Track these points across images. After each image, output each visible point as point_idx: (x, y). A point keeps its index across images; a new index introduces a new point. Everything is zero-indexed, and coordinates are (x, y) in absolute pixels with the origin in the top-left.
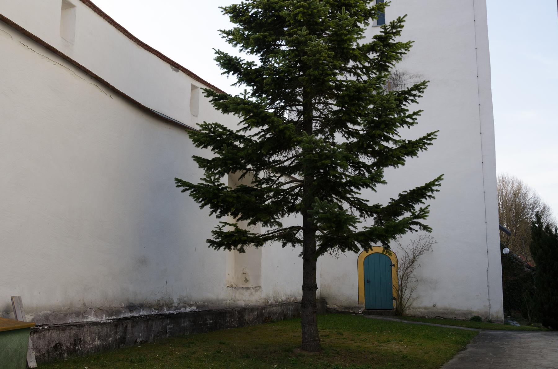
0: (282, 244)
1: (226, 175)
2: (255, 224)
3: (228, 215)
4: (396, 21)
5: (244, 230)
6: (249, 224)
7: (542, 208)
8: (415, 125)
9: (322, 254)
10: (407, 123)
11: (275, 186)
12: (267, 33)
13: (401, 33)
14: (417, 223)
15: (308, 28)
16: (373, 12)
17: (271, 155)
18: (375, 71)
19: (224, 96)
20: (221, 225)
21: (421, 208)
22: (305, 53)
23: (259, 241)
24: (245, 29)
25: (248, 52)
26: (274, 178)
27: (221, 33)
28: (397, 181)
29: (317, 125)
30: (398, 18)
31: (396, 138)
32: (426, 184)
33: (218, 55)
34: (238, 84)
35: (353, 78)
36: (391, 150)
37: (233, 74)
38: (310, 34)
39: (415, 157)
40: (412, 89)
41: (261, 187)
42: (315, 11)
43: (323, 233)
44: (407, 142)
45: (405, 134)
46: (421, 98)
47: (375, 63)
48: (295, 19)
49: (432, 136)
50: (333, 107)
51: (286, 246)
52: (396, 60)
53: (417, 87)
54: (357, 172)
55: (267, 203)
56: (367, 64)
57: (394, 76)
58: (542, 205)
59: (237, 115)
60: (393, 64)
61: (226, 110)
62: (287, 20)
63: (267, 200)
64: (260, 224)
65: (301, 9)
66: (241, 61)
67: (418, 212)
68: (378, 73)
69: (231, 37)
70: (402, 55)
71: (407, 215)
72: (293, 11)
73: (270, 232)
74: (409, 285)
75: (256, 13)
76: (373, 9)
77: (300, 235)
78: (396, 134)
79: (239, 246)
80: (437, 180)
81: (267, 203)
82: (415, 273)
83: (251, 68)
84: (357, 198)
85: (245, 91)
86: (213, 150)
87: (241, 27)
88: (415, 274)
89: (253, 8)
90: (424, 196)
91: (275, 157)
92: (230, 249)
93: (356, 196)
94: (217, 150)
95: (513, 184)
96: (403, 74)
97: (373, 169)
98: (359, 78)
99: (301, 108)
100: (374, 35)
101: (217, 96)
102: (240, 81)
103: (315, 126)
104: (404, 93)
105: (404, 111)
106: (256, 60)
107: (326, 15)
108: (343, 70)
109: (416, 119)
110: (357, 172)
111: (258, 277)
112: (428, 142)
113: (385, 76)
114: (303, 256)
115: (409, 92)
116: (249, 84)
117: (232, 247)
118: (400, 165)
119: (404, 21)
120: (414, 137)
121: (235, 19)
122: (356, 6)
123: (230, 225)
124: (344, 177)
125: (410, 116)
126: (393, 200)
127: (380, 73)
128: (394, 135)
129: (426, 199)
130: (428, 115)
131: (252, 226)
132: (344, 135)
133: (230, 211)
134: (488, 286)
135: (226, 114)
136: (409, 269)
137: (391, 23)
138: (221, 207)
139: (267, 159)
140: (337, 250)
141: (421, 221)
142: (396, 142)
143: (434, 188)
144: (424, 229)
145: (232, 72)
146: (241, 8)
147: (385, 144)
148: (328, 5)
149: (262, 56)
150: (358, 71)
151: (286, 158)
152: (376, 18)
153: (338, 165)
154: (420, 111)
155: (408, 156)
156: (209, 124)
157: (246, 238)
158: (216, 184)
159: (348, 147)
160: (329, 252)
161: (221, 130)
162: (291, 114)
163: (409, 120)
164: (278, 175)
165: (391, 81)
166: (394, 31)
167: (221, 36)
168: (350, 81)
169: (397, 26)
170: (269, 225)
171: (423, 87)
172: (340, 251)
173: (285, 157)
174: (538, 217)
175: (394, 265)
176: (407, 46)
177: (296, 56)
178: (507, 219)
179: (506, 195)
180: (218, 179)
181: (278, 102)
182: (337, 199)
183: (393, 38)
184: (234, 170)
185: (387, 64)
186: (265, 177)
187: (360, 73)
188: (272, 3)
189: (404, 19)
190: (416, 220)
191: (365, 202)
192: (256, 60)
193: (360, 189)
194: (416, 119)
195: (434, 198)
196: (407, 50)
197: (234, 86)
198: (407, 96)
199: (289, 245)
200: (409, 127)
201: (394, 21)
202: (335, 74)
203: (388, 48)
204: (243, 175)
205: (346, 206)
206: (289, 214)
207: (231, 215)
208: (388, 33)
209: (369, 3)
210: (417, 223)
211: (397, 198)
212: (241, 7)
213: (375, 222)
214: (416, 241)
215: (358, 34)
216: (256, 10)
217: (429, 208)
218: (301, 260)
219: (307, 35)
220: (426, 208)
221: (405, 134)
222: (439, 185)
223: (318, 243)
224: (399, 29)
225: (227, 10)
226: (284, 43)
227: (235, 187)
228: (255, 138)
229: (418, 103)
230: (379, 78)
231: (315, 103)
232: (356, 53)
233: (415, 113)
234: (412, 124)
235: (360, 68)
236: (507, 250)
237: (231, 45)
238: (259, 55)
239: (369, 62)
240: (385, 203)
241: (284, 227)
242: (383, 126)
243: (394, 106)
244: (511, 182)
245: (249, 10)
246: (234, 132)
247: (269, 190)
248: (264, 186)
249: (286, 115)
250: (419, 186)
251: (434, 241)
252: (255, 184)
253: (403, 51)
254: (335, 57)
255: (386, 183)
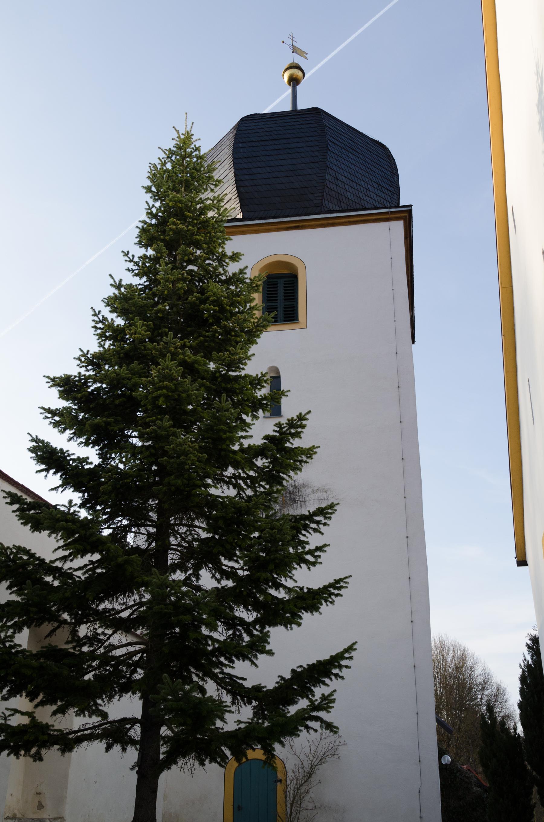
0: (105, 746)
1: (26, 631)
2: (63, 713)
3: (21, 696)
4: (295, 418)
5: (44, 723)
6: (54, 713)
7: (495, 690)
8: (317, 565)
9: (169, 768)
10: (307, 562)
11: (102, 650)
12: (111, 419)
13: (302, 435)
14: (317, 719)
15: (172, 418)
16: (265, 402)
17: (101, 600)
18: (263, 483)
19: (39, 503)
20: (8, 713)
21: (323, 695)
22: (165, 453)
23: (68, 742)
24: (80, 410)
25: (81, 443)
26: (101, 637)
27: (49, 380)
28: (290, 649)
29: (175, 557)
30: (298, 414)
31: (290, 584)
32: (331, 656)
33: (35, 444)
34: (60, 489)
35: (232, 492)
36: (282, 600)
37: (54, 473)
38: (174, 426)
39: (316, 614)
40: (315, 514)
41: (80, 650)
42: (184, 395)
43: (172, 731)
44: (306, 590)
45: (304, 578)
46: (326, 527)
47: (263, 472)
48: (154, 404)
49: (342, 584)
50: (200, 531)
51: (111, 751)
52: (293, 471)
53: (321, 511)
54: (231, 632)
55: (86, 677)
56: (252, 473)
57: (291, 489)
58: (494, 685)
59: (54, 535)
60: (289, 476)
61: (37, 526)
62: (142, 403)
63: (88, 673)
64: (72, 711)
65: (164, 391)
66: (69, 455)
67: (319, 701)
68: (267, 487)
69: (57, 418)
70: (303, 464)
71: (303, 703)
72: (153, 392)
73: (88, 726)
74: (303, 814)
75: (97, 389)
76: (265, 398)
77: (136, 732)
78: (291, 578)
79: (34, 750)
80: (346, 651)
81: (86, 677)
82: (313, 794)
83: (83, 467)
84: (228, 674)
85: (70, 501)
86: (9, 588)
87: (74, 407)
88: (313, 795)
89: (95, 382)
90: (328, 674)
91: (106, 605)
92: (17, 755)
93: (227, 670)
94: (15, 589)
95: (454, 651)
96: (304, 486)
97: (255, 629)
98: (241, 492)
99: (153, 530)
100: (264, 435)
101: (26, 503)
102: (64, 485)
103: (172, 557)
104: (304, 517)
105: (303, 543)
106: (92, 455)
107: (199, 401)
108: (219, 480)
109: (319, 556)
110: (231, 632)
111: (60, 800)
112: (336, 592)
113: (278, 491)
114: (137, 769)
115: (310, 517)
116: (77, 489)
117: (22, 752)
118: (294, 626)
119: (307, 419)
120: (316, 585)
121: (64, 395)
122: (242, 393)
123: (23, 714)
124: (210, 642)
125: (311, 552)
126: (282, 678)
127: (271, 487)
128: (288, 579)
129: (331, 679)
130: (338, 551)
131: (59, 715)
132: (213, 576)
133: (25, 688)
134: (421, 817)
135: (36, 533)
136: (304, 788)
137: (288, 420)
138: (12, 681)
139: (94, 606)
140: (191, 761)
141: (322, 714)
142: (289, 590)
143: (344, 663)
144: (327, 728)
145: (54, 470)
146: (76, 381)
147: (273, 592)
148: (203, 388)
149: (100, 449)
150: (240, 482)
151: (124, 607)
152: (268, 411)
153: (202, 622)
154: (325, 545)
155: (306, 611)
156: (8, 548)
157: (46, 737)
158: (7, 644)
159: (220, 593)
160: (180, 764)
161: (25, 558)
162: (136, 539)
163: (309, 557)
164: (109, 632)
165: (287, 495)
166: (293, 431)
167: (43, 416)
168: (227, 497)
169: (297, 425)
170: (86, 713)
171: (330, 511)
172: (197, 763)
173: (123, 605)
174: (490, 709)
175: (280, 781)
176: (310, 452)
177: (152, 455)
178: (447, 706)
179: (445, 668)
180: (12, 637)
181: (119, 519)
182: (197, 675)
183: (291, 440)
184: (39, 624)
185: (281, 475)
186: (89, 634)
187: (243, 485)
188: (124, 379)
189: (307, 417)
190: (315, 714)
191: (241, 681)
192: (92, 455)
193: (233, 662)
194: (319, 556)
195: (342, 678)
196: (310, 457)
197: (55, 491)
198: (307, 522)
199: (117, 748)
200: (309, 568)
201: (292, 418)
202: (207, 486)
203: (283, 454)
204: (53, 631)
205: (211, 688)
206: (121, 696)
207: (27, 696)
208: (285, 433)
209: (259, 389)
210: (317, 719)
211: (288, 675)
212: (77, 379)
213: (254, 713)
214: (315, 741)
215: (243, 430)
216: (99, 385)
217: (336, 696)
218: (134, 777)
219: (169, 427)
220: (331, 694)
221: (304, 578)
222: (351, 658)
223: (163, 749)
224: (299, 430)
225: (55, 382)
226: (135, 434)
227: (39, 649)
228: (79, 573)
229: (322, 534)
230: (269, 493)
231: (175, 524)
232: (238, 457)
233: (319, 549)
234: (314, 564)
235: (243, 479)
236: (447, 759)
237: (56, 430)
238: (97, 448)
239: (255, 471)
240: (270, 684)
241: (111, 718)
242: (271, 566)
243: (289, 538)
244: (452, 649)
245: (89, 384)
246: (47, 561)
247: (92, 656)
248: (85, 649)
249: (130, 538)
250: (322, 659)
251: (342, 743)
252: (70, 646)
253: (304, 458)
254: (208, 461)
255: (273, 654)
